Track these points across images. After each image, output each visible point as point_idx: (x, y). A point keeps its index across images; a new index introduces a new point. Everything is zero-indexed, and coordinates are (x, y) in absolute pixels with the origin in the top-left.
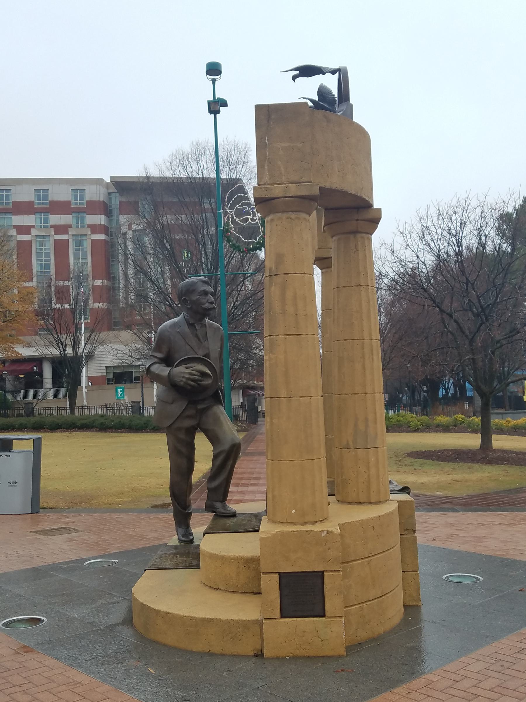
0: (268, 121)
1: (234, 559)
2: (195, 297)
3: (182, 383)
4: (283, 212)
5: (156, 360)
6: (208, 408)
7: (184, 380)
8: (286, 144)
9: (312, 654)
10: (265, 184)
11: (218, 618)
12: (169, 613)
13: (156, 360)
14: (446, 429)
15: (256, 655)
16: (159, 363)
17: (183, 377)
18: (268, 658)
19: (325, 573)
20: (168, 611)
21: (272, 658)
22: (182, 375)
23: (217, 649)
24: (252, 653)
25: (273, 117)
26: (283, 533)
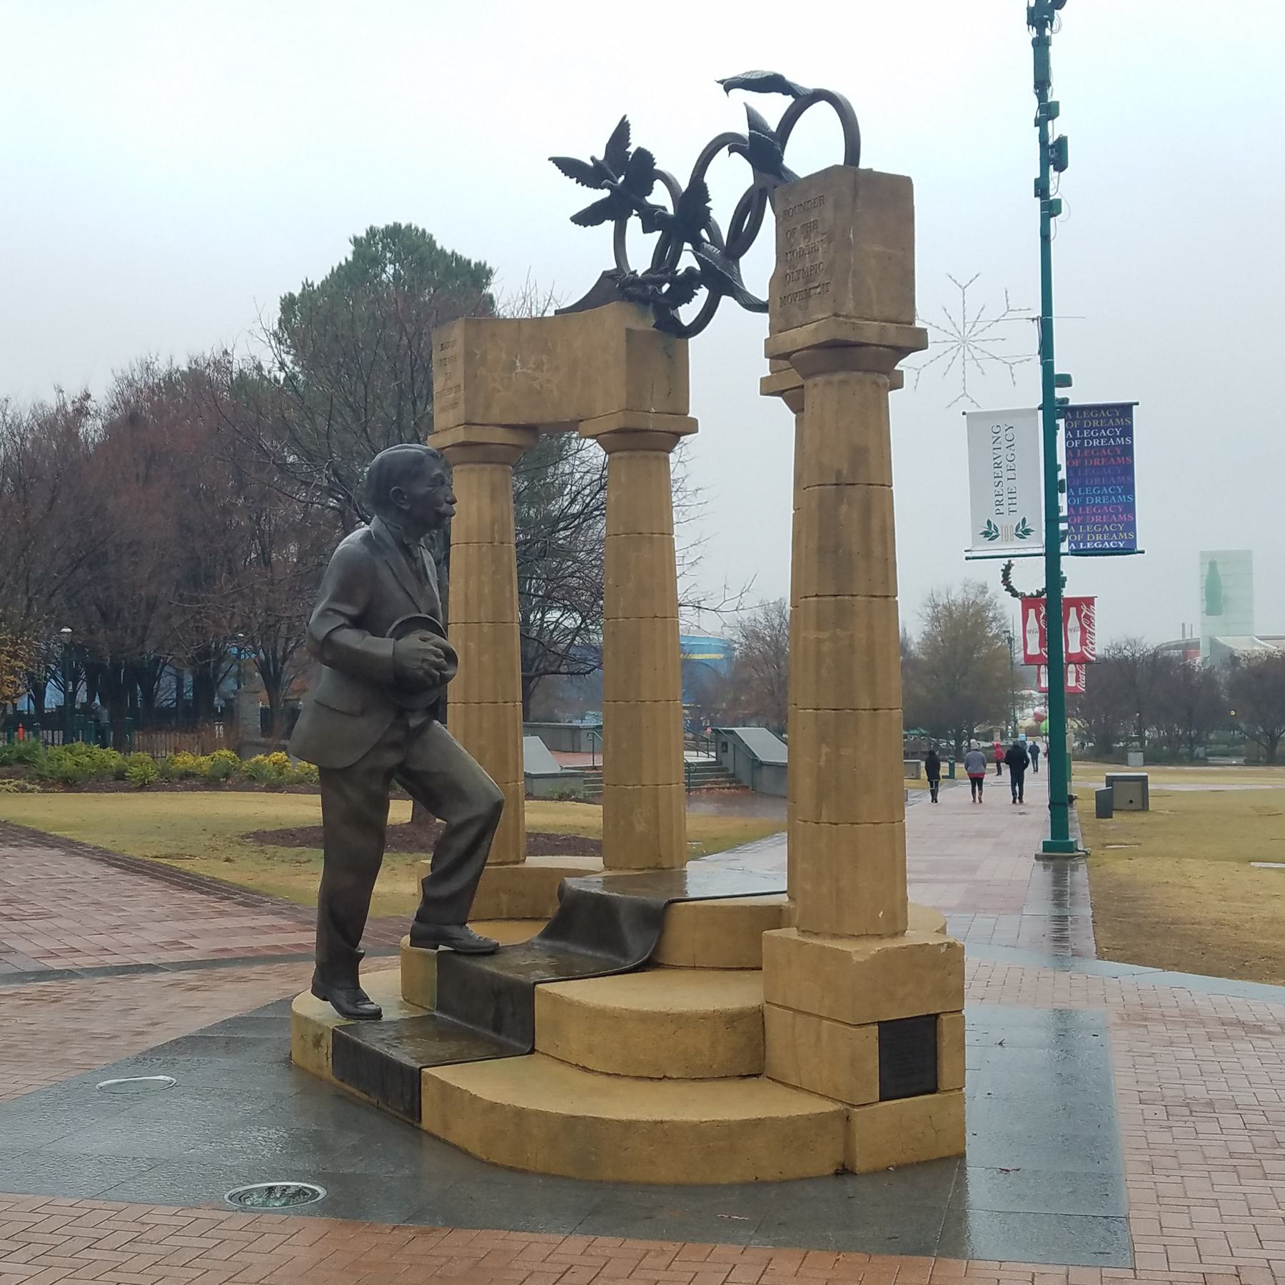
0: (854, 200)
1: (705, 1017)
2: (422, 489)
3: (421, 673)
4: (866, 371)
5: (342, 620)
6: (423, 728)
7: (425, 666)
8: (878, 248)
9: (923, 1159)
10: (846, 316)
11: (773, 1115)
12: (662, 1122)
13: (342, 620)
14: (213, 782)
15: (837, 1173)
16: (349, 628)
17: (424, 660)
18: (862, 1174)
19: (943, 1017)
20: (659, 1118)
21: (875, 1172)
22: (421, 656)
23: (770, 1174)
24: (832, 1171)
25: (861, 193)
26: (886, 953)
